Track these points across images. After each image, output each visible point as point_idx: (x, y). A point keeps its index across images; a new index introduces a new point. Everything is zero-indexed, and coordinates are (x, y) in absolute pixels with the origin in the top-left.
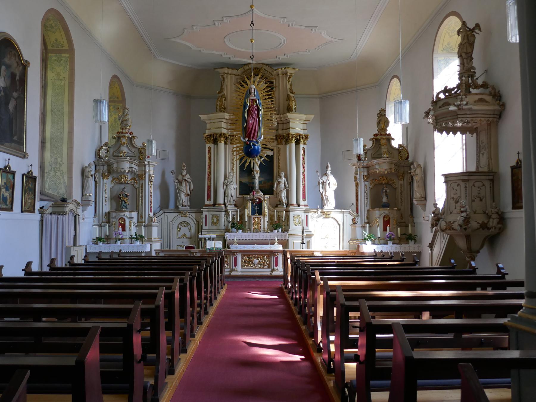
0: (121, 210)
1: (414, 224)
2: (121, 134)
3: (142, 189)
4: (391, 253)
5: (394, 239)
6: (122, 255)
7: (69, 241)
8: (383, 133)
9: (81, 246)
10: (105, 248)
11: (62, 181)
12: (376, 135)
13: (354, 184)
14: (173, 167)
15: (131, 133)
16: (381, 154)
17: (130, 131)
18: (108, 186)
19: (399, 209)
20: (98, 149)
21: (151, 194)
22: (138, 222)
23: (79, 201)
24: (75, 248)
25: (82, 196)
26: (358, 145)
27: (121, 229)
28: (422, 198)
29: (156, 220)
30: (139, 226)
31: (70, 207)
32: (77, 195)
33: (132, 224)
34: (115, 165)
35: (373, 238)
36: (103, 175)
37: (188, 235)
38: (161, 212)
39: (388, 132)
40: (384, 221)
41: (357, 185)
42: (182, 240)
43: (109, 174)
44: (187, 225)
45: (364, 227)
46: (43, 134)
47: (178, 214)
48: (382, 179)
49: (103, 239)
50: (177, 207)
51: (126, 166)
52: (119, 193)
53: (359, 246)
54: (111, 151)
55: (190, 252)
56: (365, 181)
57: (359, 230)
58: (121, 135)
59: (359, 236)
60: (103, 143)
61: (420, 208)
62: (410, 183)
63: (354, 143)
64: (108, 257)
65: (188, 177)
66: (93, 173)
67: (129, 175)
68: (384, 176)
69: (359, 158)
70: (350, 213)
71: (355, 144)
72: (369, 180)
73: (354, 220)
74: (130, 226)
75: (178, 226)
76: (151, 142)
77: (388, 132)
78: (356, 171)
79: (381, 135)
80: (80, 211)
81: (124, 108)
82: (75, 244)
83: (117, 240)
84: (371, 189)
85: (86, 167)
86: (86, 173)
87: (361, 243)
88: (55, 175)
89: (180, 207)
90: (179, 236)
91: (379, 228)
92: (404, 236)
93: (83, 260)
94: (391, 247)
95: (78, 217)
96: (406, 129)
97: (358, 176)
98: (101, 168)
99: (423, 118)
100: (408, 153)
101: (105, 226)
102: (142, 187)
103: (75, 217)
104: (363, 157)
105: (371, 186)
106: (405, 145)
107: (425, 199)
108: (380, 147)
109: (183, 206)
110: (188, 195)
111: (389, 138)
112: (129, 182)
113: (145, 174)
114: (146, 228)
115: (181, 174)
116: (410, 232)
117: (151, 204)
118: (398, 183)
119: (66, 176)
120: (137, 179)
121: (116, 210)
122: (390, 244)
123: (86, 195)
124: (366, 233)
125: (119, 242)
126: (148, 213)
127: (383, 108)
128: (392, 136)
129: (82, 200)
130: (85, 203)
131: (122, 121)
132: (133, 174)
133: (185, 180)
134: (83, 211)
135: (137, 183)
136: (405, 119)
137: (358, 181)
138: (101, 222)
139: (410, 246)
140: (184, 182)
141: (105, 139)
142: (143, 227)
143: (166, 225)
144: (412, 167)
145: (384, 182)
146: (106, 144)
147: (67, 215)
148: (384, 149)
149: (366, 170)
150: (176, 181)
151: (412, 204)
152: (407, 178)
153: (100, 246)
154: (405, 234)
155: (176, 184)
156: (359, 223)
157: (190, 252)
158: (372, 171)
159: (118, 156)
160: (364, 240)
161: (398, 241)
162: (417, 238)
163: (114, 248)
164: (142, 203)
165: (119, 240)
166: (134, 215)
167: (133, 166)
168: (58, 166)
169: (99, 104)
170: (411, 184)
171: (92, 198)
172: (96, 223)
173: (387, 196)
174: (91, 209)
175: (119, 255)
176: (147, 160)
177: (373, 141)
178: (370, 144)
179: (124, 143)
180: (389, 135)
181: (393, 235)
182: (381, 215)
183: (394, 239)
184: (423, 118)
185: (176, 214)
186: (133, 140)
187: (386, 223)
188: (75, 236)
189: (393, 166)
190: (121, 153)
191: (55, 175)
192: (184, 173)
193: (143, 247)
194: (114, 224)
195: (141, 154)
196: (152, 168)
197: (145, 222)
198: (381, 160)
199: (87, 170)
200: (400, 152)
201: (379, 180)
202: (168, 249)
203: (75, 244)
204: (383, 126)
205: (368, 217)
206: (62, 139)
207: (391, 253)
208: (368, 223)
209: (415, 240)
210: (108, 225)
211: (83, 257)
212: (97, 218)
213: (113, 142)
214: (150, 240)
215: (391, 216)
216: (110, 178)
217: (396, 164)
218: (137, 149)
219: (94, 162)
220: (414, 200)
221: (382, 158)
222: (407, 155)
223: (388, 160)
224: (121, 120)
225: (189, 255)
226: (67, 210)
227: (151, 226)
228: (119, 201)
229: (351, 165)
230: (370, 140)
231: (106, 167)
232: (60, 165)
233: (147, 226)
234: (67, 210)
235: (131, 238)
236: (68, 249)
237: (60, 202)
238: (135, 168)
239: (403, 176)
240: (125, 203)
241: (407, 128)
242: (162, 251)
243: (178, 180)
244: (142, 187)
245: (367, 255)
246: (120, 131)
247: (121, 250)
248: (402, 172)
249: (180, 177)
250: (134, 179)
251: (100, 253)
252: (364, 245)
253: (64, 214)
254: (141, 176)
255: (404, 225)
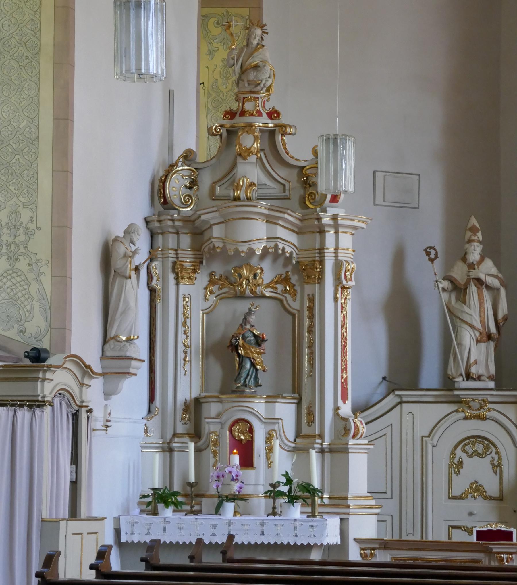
0: (239, 393)
2: (239, 121)
3: (311, 317)
6: (237, 556)
7: (53, 501)
9: (95, 519)
10: (181, 527)
11: (34, 289)
14: (434, 234)
15: (273, 114)
17: (269, 106)
18: (193, 301)
20: (161, 173)
21: (349, 338)
22: (298, 434)
23: (92, 358)
24: (74, 525)
25: (105, 341)
27: (236, 459)
29: (363, 429)
30: (299, 450)
31: (57, 380)
32: (84, 339)
33: (276, 443)
34: (217, 232)
36: (177, 269)
37: (492, 487)
38: (391, 400)
42: (469, 504)
43: (198, 263)
44: (487, 448)
47: (452, 407)
49: (175, 494)
50: (448, 383)
51: (257, 233)
52: (233, 330)
54: (206, 180)
55: (488, 552)
58: (239, 121)
60: (178, 152)
64: (183, 560)
65: (487, 270)
66: (141, 258)
67: (266, 265)
74: (270, 450)
75: (453, 454)
76: (334, 141)
80: (93, 392)
81: (255, 22)
82: (74, 513)
83: (224, 498)
85: (116, 239)
86: (117, 263)
88: (13, 268)
89: (461, 382)
90: (457, 491)
93: (92, 567)
95: (84, 415)
98: (172, 241)
101: (183, 450)
102: (313, 308)
103: (76, 416)
109: (469, 377)
110: (489, 337)
112: (267, 292)
113: (322, 262)
114: (327, 456)
115: (464, 259)
117: (345, 369)
119: (47, 270)
120: (294, 279)
121: (223, 391)
123: (115, 338)
125: (230, 507)
126: (334, 404)
129: (103, 356)
130: (115, 367)
131: (243, 71)
132: (281, 261)
133: (479, 282)
134: (107, 395)
135: (294, 294)
138: (169, 436)
140: (473, 288)
141: (189, 137)
142: (314, 454)
143: (407, 449)
146: (188, 157)
147: (48, 409)
150: (445, 284)
153: (165, 522)
155: (445, 296)
157: (488, 552)
159: (231, 199)
163: (213, 527)
164: (312, 366)
165: (233, 499)
166: (286, 411)
167: (281, 232)
168: (22, 238)
169: (133, 13)
171: (140, 348)
172: (155, 437)
174: (134, 387)
175: (224, 553)
176: (331, 211)
179: (249, 151)
185: (447, 408)
186: (279, 138)
188: (75, 485)
190: (238, 187)
191: (13, 268)
192: (474, 255)
193: (312, 528)
194: (216, 443)
195: (305, 193)
196: (346, 240)
197: (321, 436)
199: (121, 249)
202: (418, 537)
203: (74, 513)
206: (35, 141)
210: (192, 446)
211: (93, 560)
212: (156, 420)
213: (206, 149)
214: (340, 501)
216: (202, 279)
218: (295, 172)
219: (147, 222)
224: (237, 68)
225: (486, 562)
226: (47, 390)
227: (345, 450)
228: (231, 359)
231: (186, 240)
232: (29, 234)
233: (331, 451)
234: (47, 390)
235: (273, 493)
236: (50, 526)
237: (27, 362)
238: (288, 239)
240: (253, 365)
242: (385, 545)
243: (452, 281)
244: (311, 309)
246: (235, 106)
247: (231, 537)
249: (459, 272)
250: (285, 280)
251: (154, 545)
253: (35, 404)
254: (307, 269)
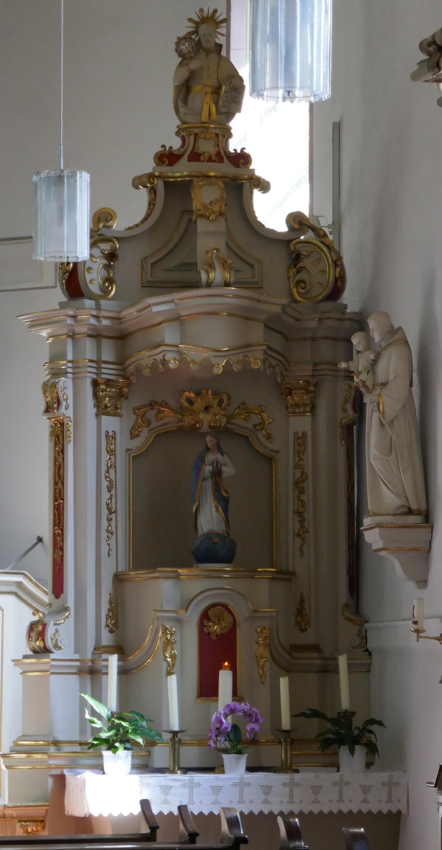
1: (365, 657)
4: (233, 823)
5: (254, 742)
8: (206, 147)
12: (166, 157)
13: (44, 425)
16: (191, 266)
19: (285, 575)
26: (65, 209)
28: (410, 512)
35: (134, 732)
39: (234, 145)
40: (204, 636)
41: (59, 436)
45: (92, 673)
46: (155, 636)
48: (199, 404)
53: (61, 781)
56: (101, 410)
57: (64, 689)
59: (65, 729)
61: (395, 566)
62: (348, 428)
63: (42, 195)
68: (206, 387)
69: (72, 281)
70: (19, 592)
71: (45, 202)
72: (126, 407)
73: (37, 630)
77: (234, 145)
78: (57, 356)
79: (195, 157)
84: (136, 458)
87: (74, 766)
91: (173, 681)
92: (313, 727)
94: (241, 785)
96: (331, 136)
97: (66, 385)
99: (415, 77)
100: (338, 262)
104: (93, 279)
105: (136, 443)
106: (325, 222)
107: (427, 517)
108: (192, 224)
111: (239, 179)
116: (345, 703)
118: (285, 428)
122: (236, 768)
124: (105, 708)
127: (208, 9)
128: (259, 167)
136: (309, 73)
137: (67, 412)
139: (341, 784)
144: (357, 340)
145: (206, 418)
148: (209, 239)
149: (108, 354)
151: (355, 544)
152: (331, 403)
154: (315, 714)
156: (66, 652)
158: (145, 358)
160: (91, 750)
161: (280, 753)
162: (380, 736)
170: (352, 434)
173: (223, 502)
177: (153, 191)
178: (132, 210)
180: (242, 159)
181: (249, 716)
182: (186, 605)
183: (254, 742)
184: (415, 77)
187: (217, 650)
189: (257, 333)
198: (189, 301)
200: (296, 258)
201: (182, 411)
204: (203, 103)
205: (118, 615)
207: (233, 823)
208: (119, 649)
209: (372, 749)
215: (241, 610)
217: (272, 325)
220: (367, 521)
221: (195, 285)
222: (332, 274)
223: (231, 297)
229: (25, 320)
230: (138, 182)
239: (312, 387)
241: (337, 128)
245: (108, 832)
248: (307, 370)
252: (88, 776)
255: (315, 660)
